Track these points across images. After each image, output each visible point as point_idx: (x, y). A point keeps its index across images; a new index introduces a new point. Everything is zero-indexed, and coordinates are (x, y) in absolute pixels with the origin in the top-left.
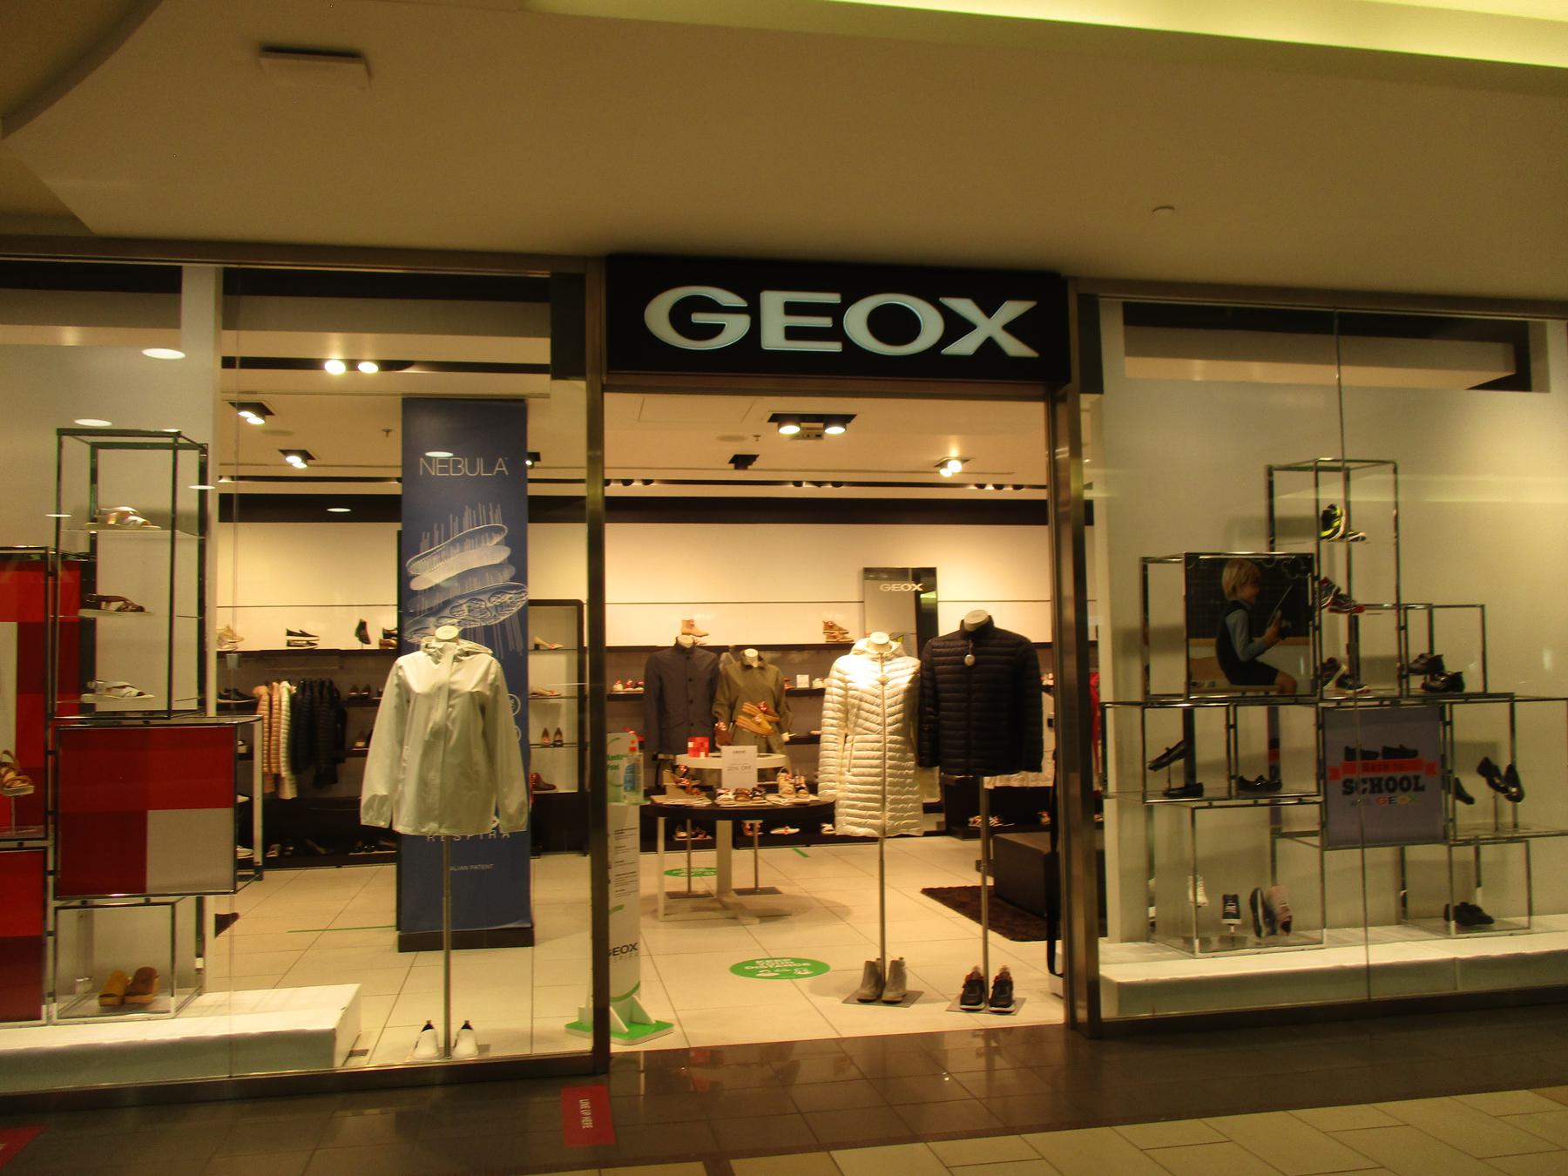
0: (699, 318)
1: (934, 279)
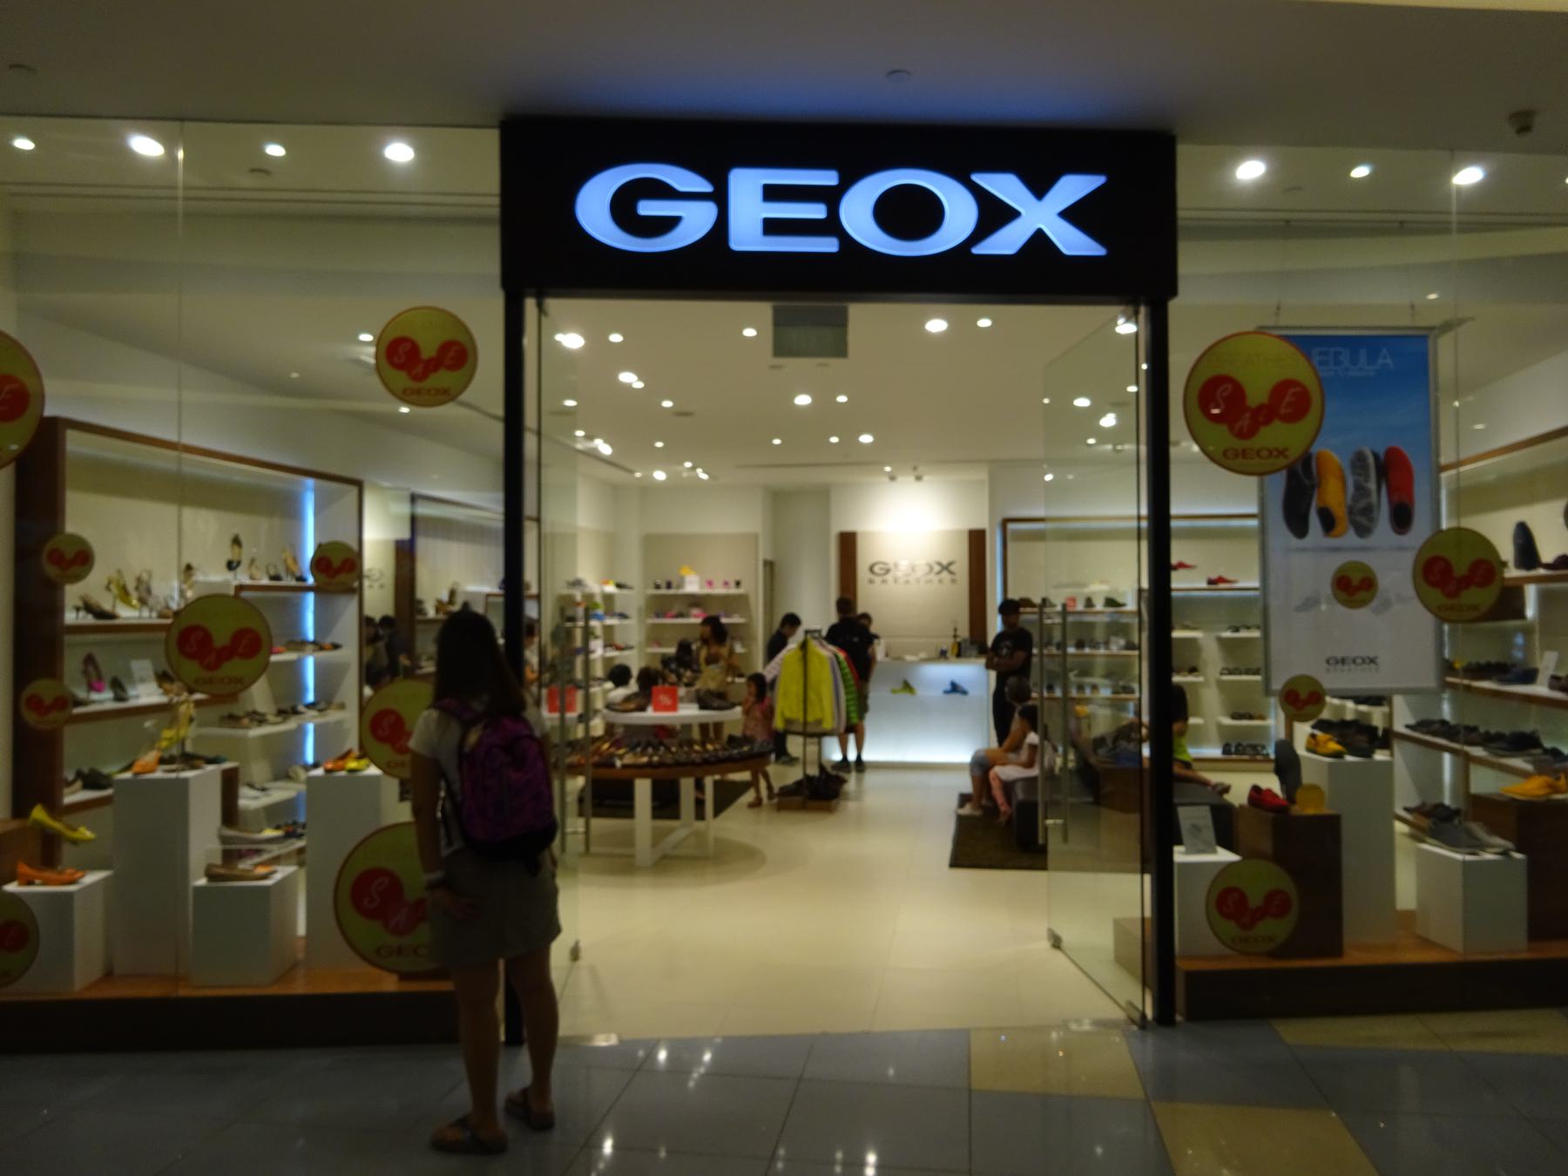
0: (648, 208)
1: (964, 147)
